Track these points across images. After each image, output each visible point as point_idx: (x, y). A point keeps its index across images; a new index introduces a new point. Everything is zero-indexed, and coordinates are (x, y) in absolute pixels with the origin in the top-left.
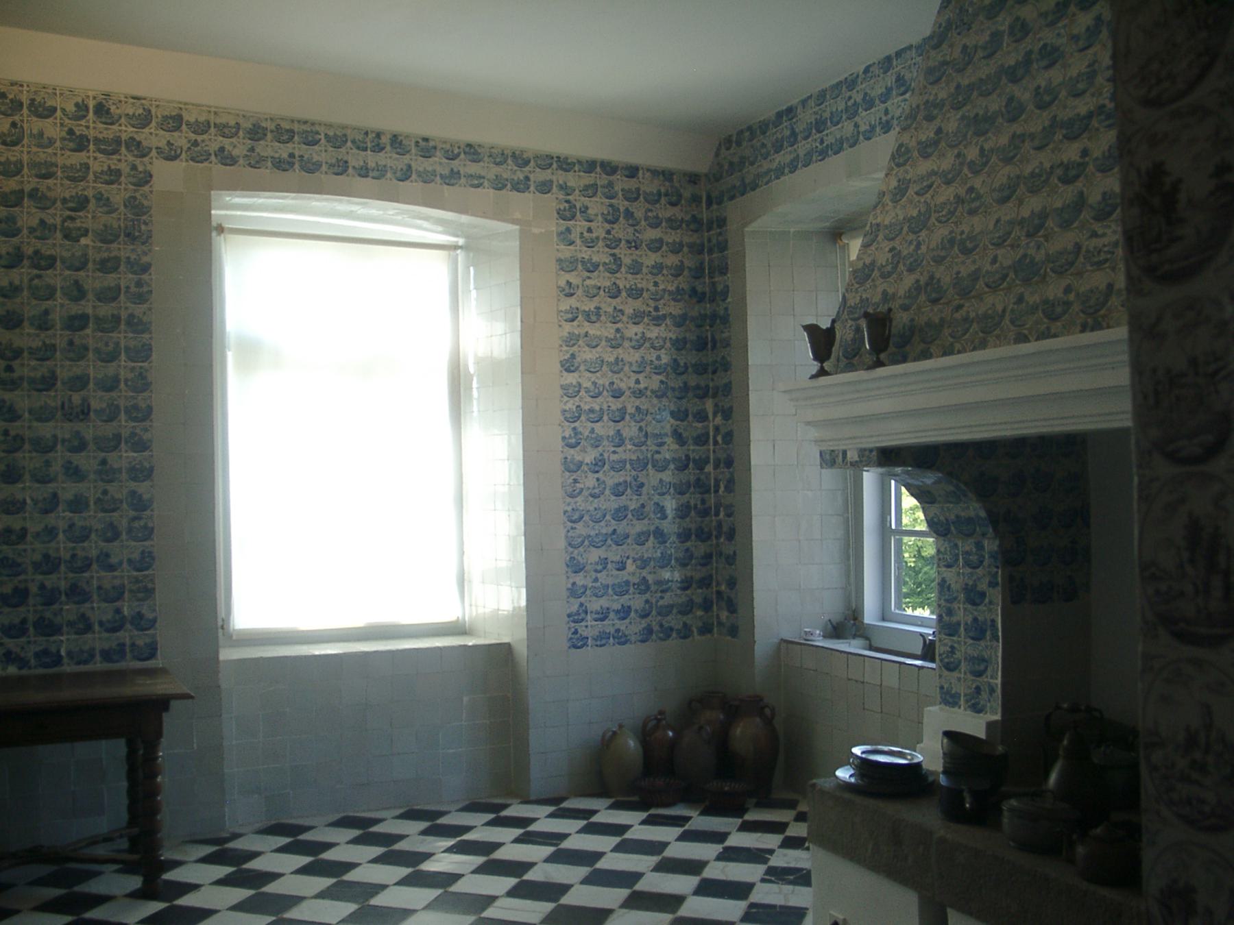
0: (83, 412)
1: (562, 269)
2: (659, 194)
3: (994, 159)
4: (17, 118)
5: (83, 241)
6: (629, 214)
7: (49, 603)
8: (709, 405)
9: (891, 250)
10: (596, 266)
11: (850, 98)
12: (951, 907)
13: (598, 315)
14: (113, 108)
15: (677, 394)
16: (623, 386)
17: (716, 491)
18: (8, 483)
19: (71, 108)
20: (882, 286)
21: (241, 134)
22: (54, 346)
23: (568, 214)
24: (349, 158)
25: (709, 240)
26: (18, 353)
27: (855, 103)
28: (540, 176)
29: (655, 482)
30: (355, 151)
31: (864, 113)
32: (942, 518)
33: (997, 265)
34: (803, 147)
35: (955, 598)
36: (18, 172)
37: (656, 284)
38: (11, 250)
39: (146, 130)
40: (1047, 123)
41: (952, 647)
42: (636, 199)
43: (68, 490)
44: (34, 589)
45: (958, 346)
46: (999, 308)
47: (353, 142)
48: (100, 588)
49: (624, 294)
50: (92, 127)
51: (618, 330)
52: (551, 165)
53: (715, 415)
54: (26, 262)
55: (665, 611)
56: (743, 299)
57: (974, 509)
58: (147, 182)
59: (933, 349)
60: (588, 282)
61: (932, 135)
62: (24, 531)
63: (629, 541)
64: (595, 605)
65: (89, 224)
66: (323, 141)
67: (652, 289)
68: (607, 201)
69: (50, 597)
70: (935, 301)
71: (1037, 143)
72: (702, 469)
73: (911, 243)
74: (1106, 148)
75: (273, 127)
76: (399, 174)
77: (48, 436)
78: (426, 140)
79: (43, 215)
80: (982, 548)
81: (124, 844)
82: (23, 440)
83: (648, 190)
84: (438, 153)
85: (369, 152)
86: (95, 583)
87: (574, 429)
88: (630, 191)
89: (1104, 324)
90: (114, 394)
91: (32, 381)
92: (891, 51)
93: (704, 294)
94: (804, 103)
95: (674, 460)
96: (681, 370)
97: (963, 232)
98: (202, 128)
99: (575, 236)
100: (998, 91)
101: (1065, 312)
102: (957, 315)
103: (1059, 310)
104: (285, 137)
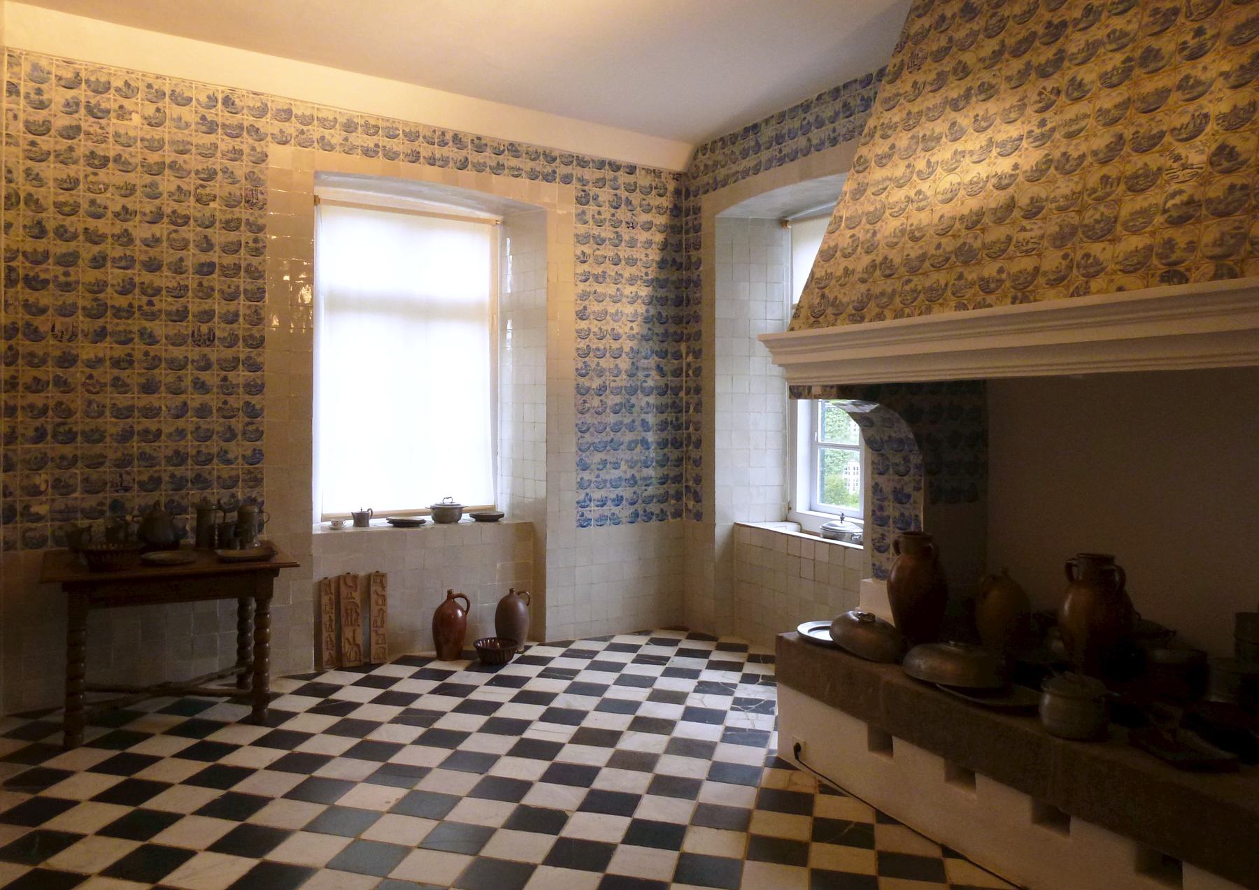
0: (209, 339)
1: (579, 242)
2: (651, 188)
3: (939, 170)
4: (160, 105)
5: (212, 205)
6: (629, 202)
7: (178, 489)
8: (683, 347)
9: (851, 237)
10: (603, 241)
11: (805, 119)
12: (897, 736)
13: (604, 277)
14: (237, 102)
15: (660, 338)
16: (621, 331)
17: (687, 412)
18: (147, 393)
19: (203, 99)
20: (844, 263)
21: (338, 126)
22: (187, 286)
23: (584, 200)
24: (421, 150)
25: (687, 224)
26: (158, 291)
27: (809, 123)
28: (563, 170)
29: (643, 404)
30: (425, 144)
31: (816, 131)
32: (878, 438)
33: (941, 250)
34: (765, 155)
35: (886, 498)
36: (161, 148)
37: (647, 255)
38: (153, 210)
39: (263, 120)
40: (984, 143)
41: (883, 535)
42: (634, 191)
43: (195, 400)
44: (166, 478)
45: (907, 311)
46: (943, 283)
47: (424, 137)
48: (219, 477)
49: (623, 262)
50: (220, 114)
51: (618, 289)
52: (572, 162)
53: (687, 354)
54: (165, 220)
55: (648, 500)
56: (712, 271)
57: (903, 430)
58: (264, 161)
59: (887, 312)
60: (597, 253)
61: (887, 150)
62: (159, 433)
63: (622, 447)
64: (597, 495)
65: (217, 192)
66: (401, 135)
67: (644, 259)
68: (613, 192)
69: (179, 484)
70: (888, 276)
71: (975, 158)
72: (677, 395)
73: (868, 231)
74: (1034, 164)
75: (363, 123)
76: (458, 164)
77: (181, 357)
78: (479, 138)
79: (179, 182)
80: (909, 461)
81: (234, 680)
82: (160, 360)
83: (643, 184)
84: (488, 150)
85: (436, 146)
86: (215, 473)
87: (585, 362)
88: (629, 184)
89: (1032, 298)
90: (235, 326)
91: (168, 313)
92: (841, 84)
93: (681, 264)
94: (767, 121)
95: (657, 388)
96: (663, 320)
97: (912, 225)
98: (307, 120)
99: (588, 217)
100: (943, 117)
101: (998, 287)
102: (907, 288)
103: (992, 286)
104: (372, 131)
